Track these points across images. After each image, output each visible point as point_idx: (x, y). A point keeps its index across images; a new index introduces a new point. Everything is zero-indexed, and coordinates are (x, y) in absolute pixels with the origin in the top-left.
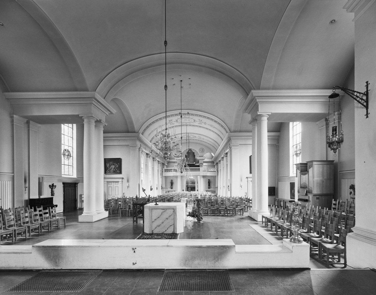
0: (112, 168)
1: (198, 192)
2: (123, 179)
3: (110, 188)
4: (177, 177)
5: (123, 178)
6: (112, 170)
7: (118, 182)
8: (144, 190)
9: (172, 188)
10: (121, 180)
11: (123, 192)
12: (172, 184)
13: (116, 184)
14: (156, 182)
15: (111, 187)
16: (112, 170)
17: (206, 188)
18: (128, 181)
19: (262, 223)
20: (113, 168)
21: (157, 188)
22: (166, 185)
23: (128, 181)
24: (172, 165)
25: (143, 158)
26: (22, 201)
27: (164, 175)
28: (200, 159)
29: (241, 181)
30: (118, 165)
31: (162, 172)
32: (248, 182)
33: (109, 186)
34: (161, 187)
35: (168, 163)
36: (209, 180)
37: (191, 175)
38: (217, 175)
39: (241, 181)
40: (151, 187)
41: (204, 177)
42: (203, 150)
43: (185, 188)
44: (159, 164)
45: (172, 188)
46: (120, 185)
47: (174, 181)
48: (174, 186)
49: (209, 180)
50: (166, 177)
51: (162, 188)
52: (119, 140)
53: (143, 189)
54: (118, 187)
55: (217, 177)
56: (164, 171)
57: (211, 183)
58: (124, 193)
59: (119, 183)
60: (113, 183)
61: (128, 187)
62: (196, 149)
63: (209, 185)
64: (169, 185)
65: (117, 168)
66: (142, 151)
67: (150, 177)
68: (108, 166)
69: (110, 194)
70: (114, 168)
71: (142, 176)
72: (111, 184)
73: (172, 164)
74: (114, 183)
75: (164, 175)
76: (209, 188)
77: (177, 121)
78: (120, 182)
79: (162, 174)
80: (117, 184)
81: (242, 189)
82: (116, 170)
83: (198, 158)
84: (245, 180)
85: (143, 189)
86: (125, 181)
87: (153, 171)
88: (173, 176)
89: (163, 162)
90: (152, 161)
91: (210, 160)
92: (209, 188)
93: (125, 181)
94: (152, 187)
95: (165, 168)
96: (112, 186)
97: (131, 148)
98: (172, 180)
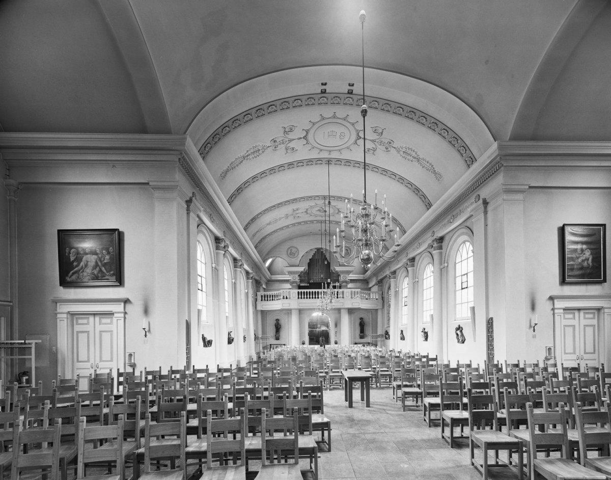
0: (86, 266)
1: (336, 346)
2: (128, 306)
3: (83, 338)
4: (288, 312)
5: (126, 301)
6: (89, 270)
7: (110, 314)
8: (207, 343)
9: (277, 339)
10: (120, 307)
11: (129, 351)
12: (278, 328)
13: (104, 321)
14: (242, 325)
15: (88, 332)
16: (89, 270)
17: (355, 338)
18: (146, 311)
19: (122, 315)
20: (91, 264)
21: (245, 338)
22: (264, 332)
23: (146, 311)
24: (272, 288)
25: (202, 252)
26: (564, 313)
27: (259, 308)
28: (344, 272)
29: (533, 308)
30: (109, 253)
31: (256, 300)
32: (556, 311)
33: (77, 328)
34: (253, 337)
35: (267, 284)
36: (361, 319)
37: (320, 308)
38: (379, 307)
39: (533, 308)
40: (229, 334)
41: (351, 311)
42: (349, 251)
43: (307, 339)
44: (248, 278)
45: (277, 339)
46: (116, 324)
47: (282, 322)
48: (283, 333)
49: (361, 319)
50: (264, 313)
51: (256, 338)
52: (113, 164)
53: (204, 339)
54: (88, 332)
55: (380, 313)
56: (259, 298)
57: (366, 327)
58: (130, 355)
59: (115, 320)
60: (91, 319)
61: (147, 332)
62: (334, 246)
63: (362, 331)
64: (271, 331)
65: (105, 265)
66: (201, 223)
67: (227, 307)
68: (72, 259)
69: (83, 356)
70: (96, 265)
71: (202, 299)
72: (85, 321)
73: (277, 285)
74: (97, 318)
75: (259, 308)
76: (362, 337)
77: (305, 138)
78: (116, 315)
79: (255, 306)
80: (108, 321)
81: (534, 337)
82: (101, 270)
83: (338, 269)
84: (544, 306)
85: (204, 339)
86: (135, 310)
87: (236, 297)
88: (282, 310)
89: (257, 278)
90: (232, 266)
91: (361, 277)
92: (362, 337)
93: (135, 310)
94: (232, 335)
95: (262, 293)
96: (89, 328)
97: (157, 194)
98: (277, 320)
